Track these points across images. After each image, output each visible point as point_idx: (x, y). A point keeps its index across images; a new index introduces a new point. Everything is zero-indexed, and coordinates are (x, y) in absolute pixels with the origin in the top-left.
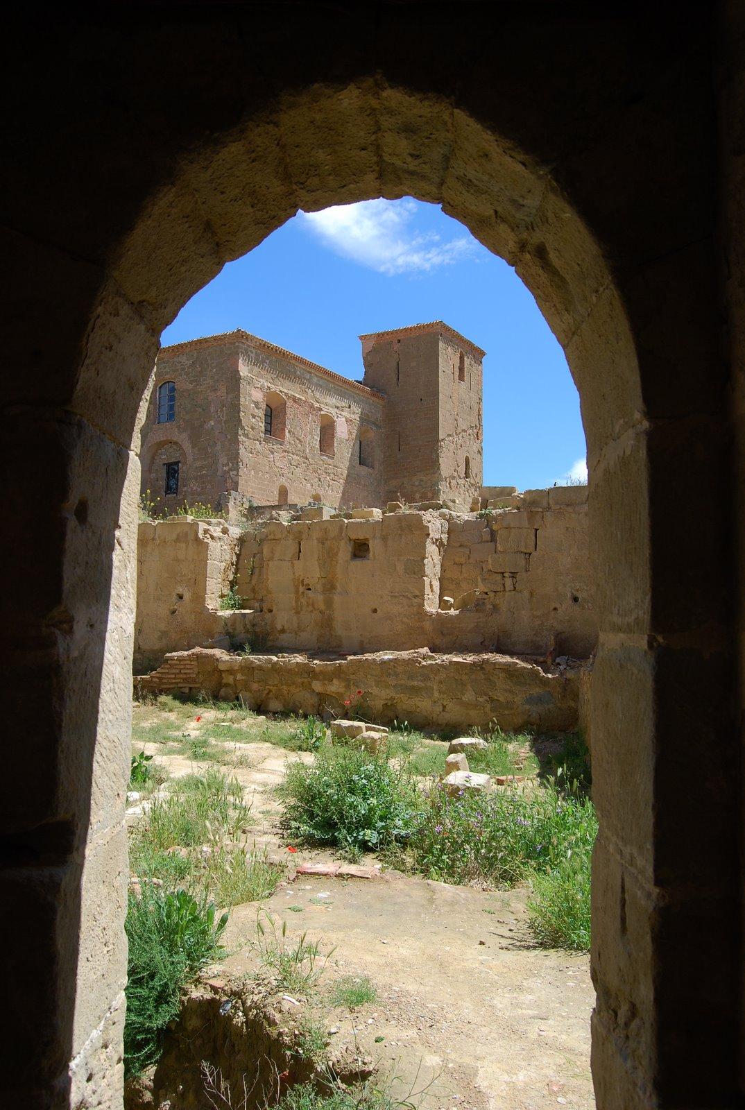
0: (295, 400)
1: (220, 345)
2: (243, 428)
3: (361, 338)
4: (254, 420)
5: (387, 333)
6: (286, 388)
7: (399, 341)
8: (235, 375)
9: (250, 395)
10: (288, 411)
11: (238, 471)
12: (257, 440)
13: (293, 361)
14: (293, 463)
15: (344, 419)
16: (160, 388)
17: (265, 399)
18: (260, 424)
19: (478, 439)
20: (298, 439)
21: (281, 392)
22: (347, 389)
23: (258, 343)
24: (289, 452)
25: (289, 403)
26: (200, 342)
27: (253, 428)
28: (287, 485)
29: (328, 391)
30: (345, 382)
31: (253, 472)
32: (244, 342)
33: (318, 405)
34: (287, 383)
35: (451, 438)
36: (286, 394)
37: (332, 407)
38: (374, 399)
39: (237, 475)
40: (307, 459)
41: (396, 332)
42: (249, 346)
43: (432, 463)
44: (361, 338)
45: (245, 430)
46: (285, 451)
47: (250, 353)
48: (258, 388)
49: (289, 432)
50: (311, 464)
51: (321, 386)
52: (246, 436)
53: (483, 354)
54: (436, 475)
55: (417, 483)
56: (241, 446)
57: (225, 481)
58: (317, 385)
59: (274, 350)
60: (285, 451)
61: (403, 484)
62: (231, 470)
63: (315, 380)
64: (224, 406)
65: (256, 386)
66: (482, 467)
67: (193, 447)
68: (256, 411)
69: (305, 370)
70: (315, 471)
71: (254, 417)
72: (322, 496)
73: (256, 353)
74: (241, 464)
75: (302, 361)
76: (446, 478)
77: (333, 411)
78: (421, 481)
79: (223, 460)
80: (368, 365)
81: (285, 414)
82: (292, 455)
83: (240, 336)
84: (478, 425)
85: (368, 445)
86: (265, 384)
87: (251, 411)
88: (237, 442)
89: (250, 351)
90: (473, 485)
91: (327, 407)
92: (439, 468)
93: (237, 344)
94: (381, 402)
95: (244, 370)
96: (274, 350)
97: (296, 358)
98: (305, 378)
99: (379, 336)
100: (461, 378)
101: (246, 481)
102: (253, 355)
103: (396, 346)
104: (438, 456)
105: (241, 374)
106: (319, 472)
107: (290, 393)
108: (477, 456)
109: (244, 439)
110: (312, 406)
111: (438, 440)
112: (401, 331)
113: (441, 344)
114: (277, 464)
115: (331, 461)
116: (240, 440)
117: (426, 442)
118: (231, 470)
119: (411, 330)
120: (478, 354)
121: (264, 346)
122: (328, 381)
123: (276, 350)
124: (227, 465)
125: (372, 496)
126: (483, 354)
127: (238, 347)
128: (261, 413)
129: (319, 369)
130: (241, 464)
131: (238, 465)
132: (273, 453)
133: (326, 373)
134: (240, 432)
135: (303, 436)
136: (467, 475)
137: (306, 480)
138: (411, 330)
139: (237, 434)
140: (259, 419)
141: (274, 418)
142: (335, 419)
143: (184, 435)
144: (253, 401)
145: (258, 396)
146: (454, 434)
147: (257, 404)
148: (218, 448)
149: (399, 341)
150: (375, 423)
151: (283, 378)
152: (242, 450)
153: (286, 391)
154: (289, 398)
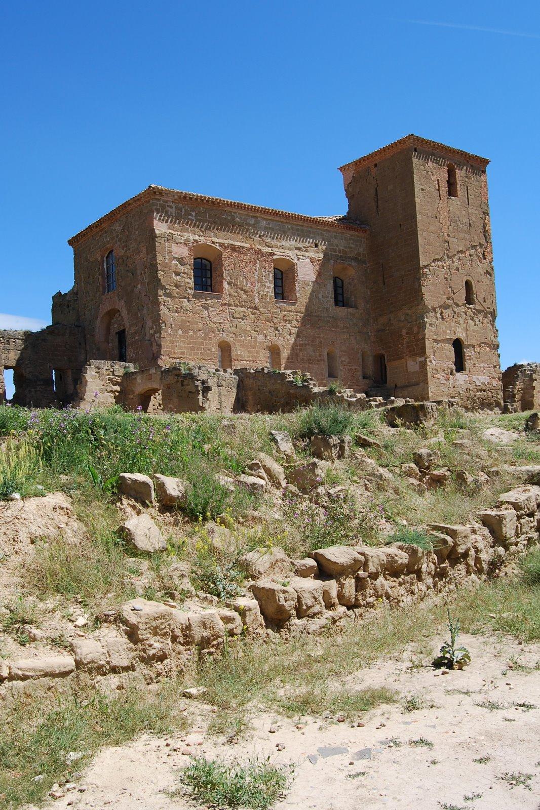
0: (234, 248)
1: (139, 205)
2: (163, 288)
3: (341, 169)
4: (178, 278)
5: (363, 159)
6: (216, 239)
7: (376, 165)
8: (152, 234)
9: (170, 252)
10: (225, 262)
11: (161, 333)
12: (185, 297)
13: (228, 209)
14: (236, 315)
15: (309, 260)
16: (107, 258)
17: (192, 253)
18: (188, 280)
19: (485, 259)
20: (242, 290)
21: (214, 243)
22: (311, 228)
23: (176, 197)
24: (230, 305)
25: (226, 254)
26: (125, 206)
27: (177, 286)
28: (230, 339)
29: (283, 233)
30: (325, 223)
31: (180, 332)
32: (159, 198)
33: (270, 250)
34: (222, 234)
35: (440, 263)
36: (221, 245)
37: (290, 250)
38: (352, 233)
39: (160, 337)
40: (257, 309)
41: (371, 156)
42: (167, 202)
43: (416, 295)
44: (341, 169)
45: (166, 289)
46: (225, 305)
47: (168, 208)
48: (181, 243)
49: (229, 283)
50: (262, 314)
51: (272, 229)
52: (169, 295)
53: (486, 162)
54: (421, 307)
55: (403, 318)
56: (162, 306)
57: (151, 345)
58: (266, 229)
59: (199, 200)
60: (225, 305)
61: (390, 320)
62: (155, 332)
63: (264, 223)
64: (146, 267)
65: (176, 244)
66: (494, 289)
67: (128, 314)
68: (182, 267)
69: (248, 215)
70: (269, 320)
71: (177, 274)
72: (281, 347)
73: (177, 208)
74: (163, 325)
75: (239, 206)
76: (434, 309)
77: (292, 255)
78: (407, 314)
79: (149, 323)
80: (350, 196)
81: (222, 265)
82: (234, 308)
83: (153, 193)
84: (484, 242)
85: (350, 283)
86: (191, 238)
87: (174, 269)
88: (157, 303)
89: (169, 206)
90: (479, 311)
91: (283, 250)
92: (422, 299)
93: (151, 201)
94: (361, 234)
95: (160, 227)
96: (199, 200)
97: (231, 205)
98: (249, 225)
99: (357, 163)
100: (452, 192)
101: (172, 342)
102: (173, 210)
103: (374, 171)
104: (420, 286)
105: (157, 232)
106: (275, 320)
107: (226, 242)
108: (486, 280)
109: (166, 299)
110: (259, 252)
111: (418, 268)
112: (376, 153)
113: (415, 160)
114: (215, 320)
115: (292, 308)
116: (160, 300)
117: (408, 271)
118: (155, 332)
119: (384, 150)
120: (478, 165)
121: (185, 198)
122: (282, 222)
123: (202, 200)
124: (152, 328)
125: (356, 338)
126: (486, 162)
127: (153, 204)
128: (189, 269)
129: (265, 211)
130: (163, 325)
131: (161, 327)
132: (207, 309)
133: (276, 214)
134: (161, 292)
135: (248, 285)
136: (469, 300)
137: (255, 331)
138: (384, 150)
139: (157, 295)
140: (185, 276)
141: (206, 274)
142: (295, 261)
143: (122, 303)
144: (175, 258)
145: (182, 251)
146: (445, 257)
147: (181, 261)
148: (145, 311)
149: (376, 165)
150: (356, 259)
151: (217, 229)
152: (163, 310)
153: (221, 241)
154: (226, 248)
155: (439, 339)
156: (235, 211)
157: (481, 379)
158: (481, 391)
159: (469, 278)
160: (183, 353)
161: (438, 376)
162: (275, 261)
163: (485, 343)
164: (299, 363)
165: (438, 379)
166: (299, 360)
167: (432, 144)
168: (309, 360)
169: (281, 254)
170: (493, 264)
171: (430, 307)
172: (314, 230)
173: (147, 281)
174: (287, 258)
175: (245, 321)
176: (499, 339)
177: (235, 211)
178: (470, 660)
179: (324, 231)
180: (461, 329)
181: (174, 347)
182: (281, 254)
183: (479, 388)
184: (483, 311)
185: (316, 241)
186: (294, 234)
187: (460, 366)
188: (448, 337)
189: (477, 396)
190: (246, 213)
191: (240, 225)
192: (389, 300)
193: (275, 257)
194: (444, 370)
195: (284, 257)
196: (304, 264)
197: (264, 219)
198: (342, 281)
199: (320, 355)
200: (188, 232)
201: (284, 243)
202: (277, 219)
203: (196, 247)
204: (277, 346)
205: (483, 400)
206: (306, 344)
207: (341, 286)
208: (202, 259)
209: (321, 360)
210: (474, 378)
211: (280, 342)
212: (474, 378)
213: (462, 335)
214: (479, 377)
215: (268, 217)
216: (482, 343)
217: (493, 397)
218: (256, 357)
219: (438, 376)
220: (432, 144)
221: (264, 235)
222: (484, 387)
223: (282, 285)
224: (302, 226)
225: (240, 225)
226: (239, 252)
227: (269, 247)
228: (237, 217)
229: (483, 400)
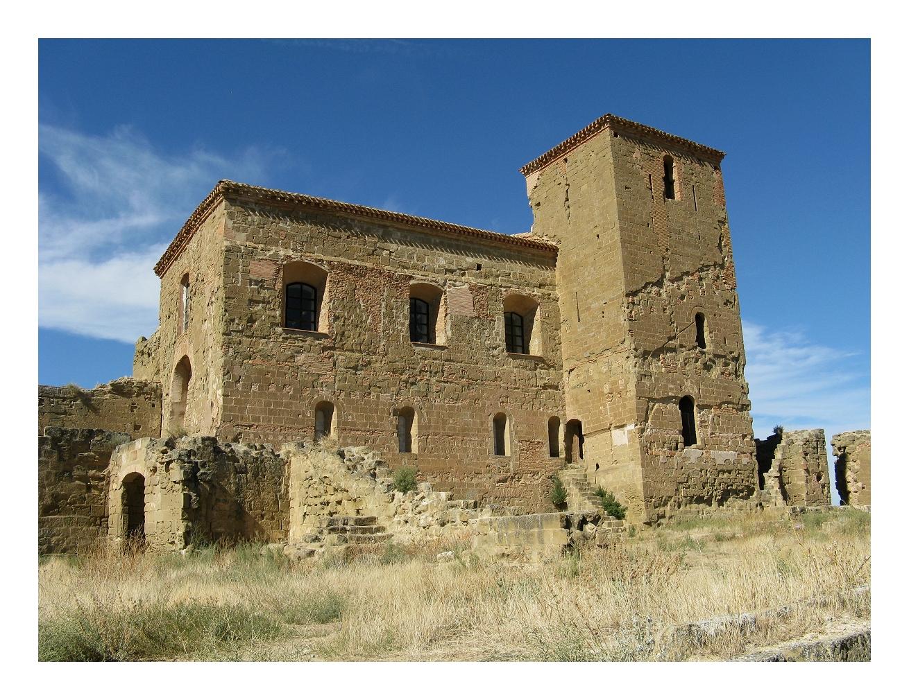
13: (342, 214)
32: (234, 197)
86: (282, 253)
157: (723, 456)
160: (257, 419)
162: (413, 287)
169: (424, 278)
170: (736, 292)
172: (476, 246)
173: (213, 314)
176: (750, 397)
177: (352, 217)
178: (101, 432)
179: (491, 247)
180: (692, 382)
181: (242, 410)
182: (424, 278)
192: (586, 343)
193: (412, 282)
197: (399, 229)
198: (522, 318)
199: (482, 424)
200: (277, 246)
203: (290, 267)
207: (520, 325)
208: (302, 284)
213: (690, 389)
216: (724, 403)
223: (428, 323)
224: (458, 240)
227: (404, 267)
228: (355, 226)
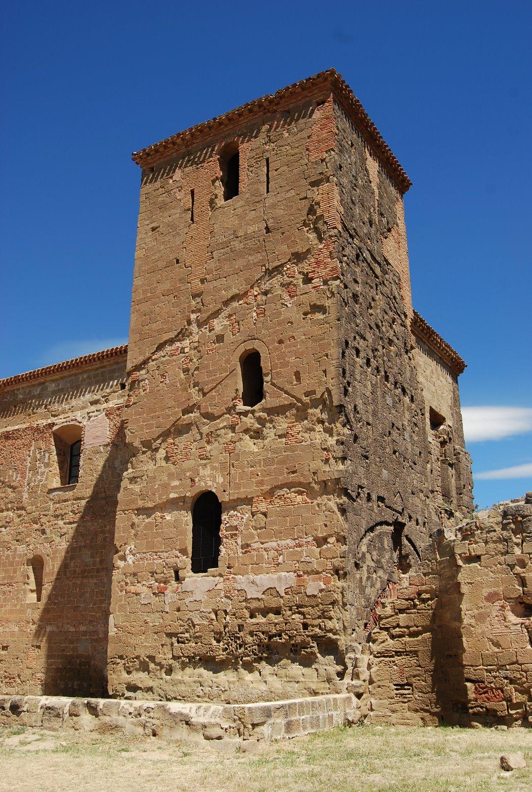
13: (9, 388)
63: (52, 387)
75: (17, 380)
129: (47, 372)
136: (254, 392)
155: (150, 505)
156: (15, 387)
158: (265, 612)
159: (256, 345)
161: (139, 588)
163: (289, 486)
164: (68, 578)
165: (137, 594)
166: (68, 574)
167: (179, 141)
168: (83, 572)
171: (137, 444)
174: (72, 423)
175: (8, 529)
177: (15, 387)
180: (213, 468)
183: (254, 605)
184: (291, 406)
185: (123, 380)
186: (90, 385)
187: (205, 556)
188: (173, 495)
189: (247, 629)
190: (28, 384)
191: (23, 402)
193: (55, 428)
194: (153, 573)
195: (69, 423)
196: (95, 423)
201: (74, 402)
202: (66, 373)
204: (40, 556)
205: (270, 637)
206: (80, 547)
209: (103, 569)
210: (242, 581)
211: (44, 550)
212: (242, 581)
213: (211, 480)
214: (258, 578)
215: (55, 377)
217: (305, 626)
218: (12, 578)
219: (139, 588)
220: (179, 141)
221: (50, 403)
222: (274, 603)
225: (23, 402)
226: (14, 438)
229: (270, 637)
